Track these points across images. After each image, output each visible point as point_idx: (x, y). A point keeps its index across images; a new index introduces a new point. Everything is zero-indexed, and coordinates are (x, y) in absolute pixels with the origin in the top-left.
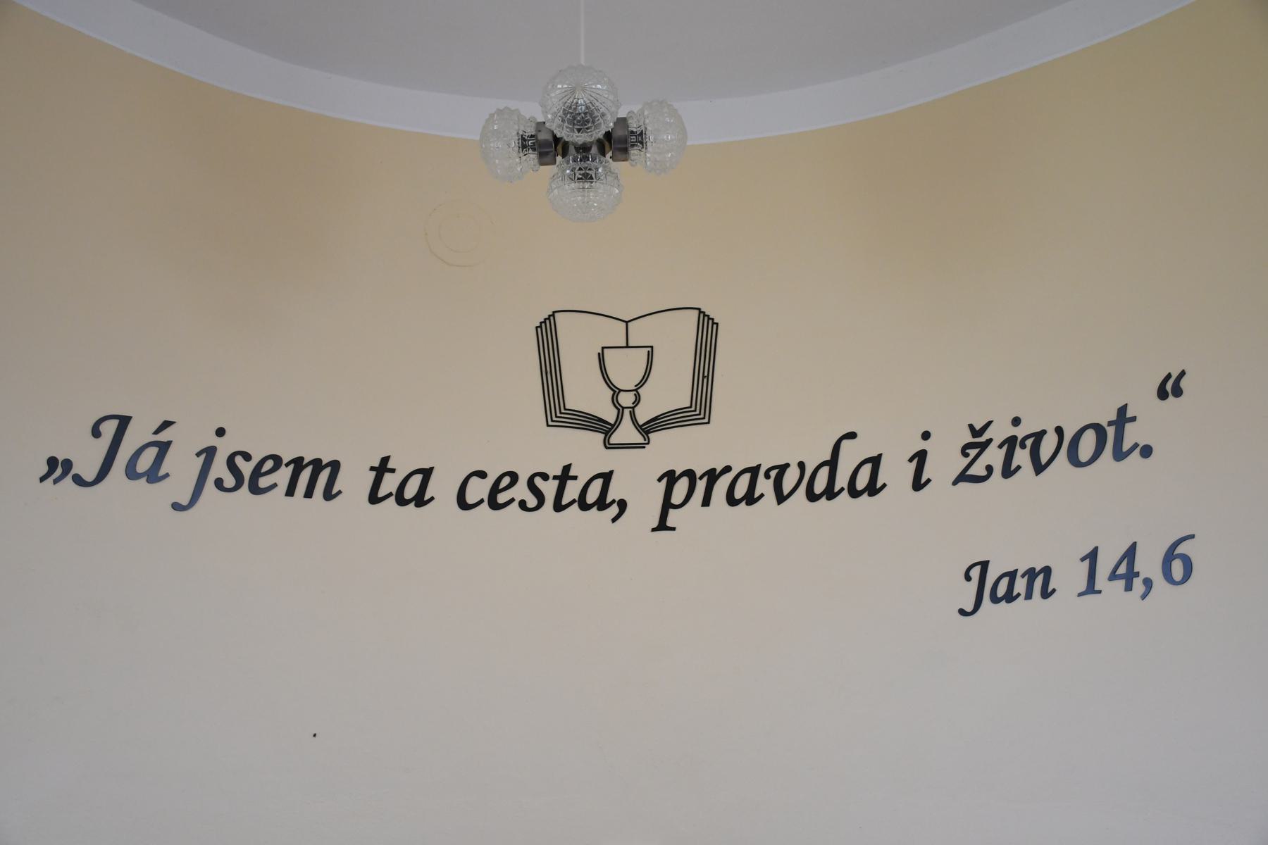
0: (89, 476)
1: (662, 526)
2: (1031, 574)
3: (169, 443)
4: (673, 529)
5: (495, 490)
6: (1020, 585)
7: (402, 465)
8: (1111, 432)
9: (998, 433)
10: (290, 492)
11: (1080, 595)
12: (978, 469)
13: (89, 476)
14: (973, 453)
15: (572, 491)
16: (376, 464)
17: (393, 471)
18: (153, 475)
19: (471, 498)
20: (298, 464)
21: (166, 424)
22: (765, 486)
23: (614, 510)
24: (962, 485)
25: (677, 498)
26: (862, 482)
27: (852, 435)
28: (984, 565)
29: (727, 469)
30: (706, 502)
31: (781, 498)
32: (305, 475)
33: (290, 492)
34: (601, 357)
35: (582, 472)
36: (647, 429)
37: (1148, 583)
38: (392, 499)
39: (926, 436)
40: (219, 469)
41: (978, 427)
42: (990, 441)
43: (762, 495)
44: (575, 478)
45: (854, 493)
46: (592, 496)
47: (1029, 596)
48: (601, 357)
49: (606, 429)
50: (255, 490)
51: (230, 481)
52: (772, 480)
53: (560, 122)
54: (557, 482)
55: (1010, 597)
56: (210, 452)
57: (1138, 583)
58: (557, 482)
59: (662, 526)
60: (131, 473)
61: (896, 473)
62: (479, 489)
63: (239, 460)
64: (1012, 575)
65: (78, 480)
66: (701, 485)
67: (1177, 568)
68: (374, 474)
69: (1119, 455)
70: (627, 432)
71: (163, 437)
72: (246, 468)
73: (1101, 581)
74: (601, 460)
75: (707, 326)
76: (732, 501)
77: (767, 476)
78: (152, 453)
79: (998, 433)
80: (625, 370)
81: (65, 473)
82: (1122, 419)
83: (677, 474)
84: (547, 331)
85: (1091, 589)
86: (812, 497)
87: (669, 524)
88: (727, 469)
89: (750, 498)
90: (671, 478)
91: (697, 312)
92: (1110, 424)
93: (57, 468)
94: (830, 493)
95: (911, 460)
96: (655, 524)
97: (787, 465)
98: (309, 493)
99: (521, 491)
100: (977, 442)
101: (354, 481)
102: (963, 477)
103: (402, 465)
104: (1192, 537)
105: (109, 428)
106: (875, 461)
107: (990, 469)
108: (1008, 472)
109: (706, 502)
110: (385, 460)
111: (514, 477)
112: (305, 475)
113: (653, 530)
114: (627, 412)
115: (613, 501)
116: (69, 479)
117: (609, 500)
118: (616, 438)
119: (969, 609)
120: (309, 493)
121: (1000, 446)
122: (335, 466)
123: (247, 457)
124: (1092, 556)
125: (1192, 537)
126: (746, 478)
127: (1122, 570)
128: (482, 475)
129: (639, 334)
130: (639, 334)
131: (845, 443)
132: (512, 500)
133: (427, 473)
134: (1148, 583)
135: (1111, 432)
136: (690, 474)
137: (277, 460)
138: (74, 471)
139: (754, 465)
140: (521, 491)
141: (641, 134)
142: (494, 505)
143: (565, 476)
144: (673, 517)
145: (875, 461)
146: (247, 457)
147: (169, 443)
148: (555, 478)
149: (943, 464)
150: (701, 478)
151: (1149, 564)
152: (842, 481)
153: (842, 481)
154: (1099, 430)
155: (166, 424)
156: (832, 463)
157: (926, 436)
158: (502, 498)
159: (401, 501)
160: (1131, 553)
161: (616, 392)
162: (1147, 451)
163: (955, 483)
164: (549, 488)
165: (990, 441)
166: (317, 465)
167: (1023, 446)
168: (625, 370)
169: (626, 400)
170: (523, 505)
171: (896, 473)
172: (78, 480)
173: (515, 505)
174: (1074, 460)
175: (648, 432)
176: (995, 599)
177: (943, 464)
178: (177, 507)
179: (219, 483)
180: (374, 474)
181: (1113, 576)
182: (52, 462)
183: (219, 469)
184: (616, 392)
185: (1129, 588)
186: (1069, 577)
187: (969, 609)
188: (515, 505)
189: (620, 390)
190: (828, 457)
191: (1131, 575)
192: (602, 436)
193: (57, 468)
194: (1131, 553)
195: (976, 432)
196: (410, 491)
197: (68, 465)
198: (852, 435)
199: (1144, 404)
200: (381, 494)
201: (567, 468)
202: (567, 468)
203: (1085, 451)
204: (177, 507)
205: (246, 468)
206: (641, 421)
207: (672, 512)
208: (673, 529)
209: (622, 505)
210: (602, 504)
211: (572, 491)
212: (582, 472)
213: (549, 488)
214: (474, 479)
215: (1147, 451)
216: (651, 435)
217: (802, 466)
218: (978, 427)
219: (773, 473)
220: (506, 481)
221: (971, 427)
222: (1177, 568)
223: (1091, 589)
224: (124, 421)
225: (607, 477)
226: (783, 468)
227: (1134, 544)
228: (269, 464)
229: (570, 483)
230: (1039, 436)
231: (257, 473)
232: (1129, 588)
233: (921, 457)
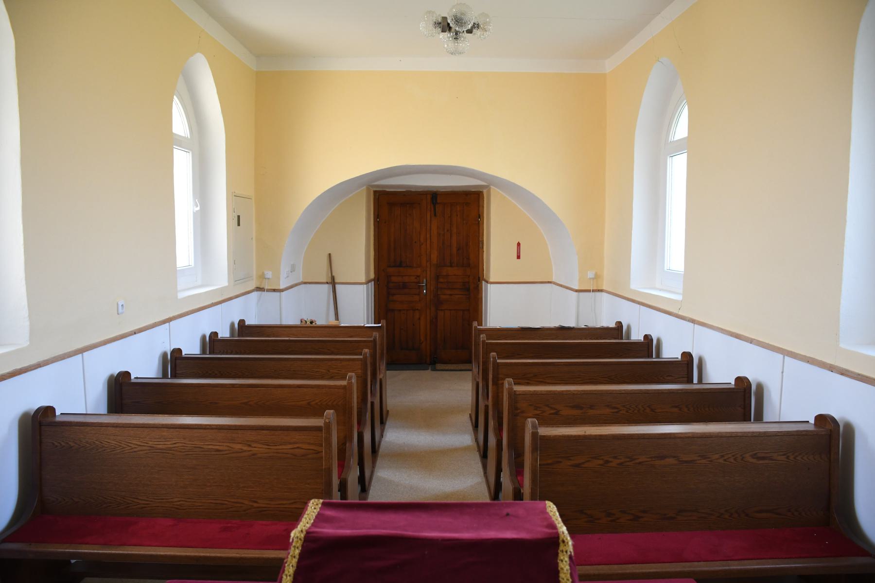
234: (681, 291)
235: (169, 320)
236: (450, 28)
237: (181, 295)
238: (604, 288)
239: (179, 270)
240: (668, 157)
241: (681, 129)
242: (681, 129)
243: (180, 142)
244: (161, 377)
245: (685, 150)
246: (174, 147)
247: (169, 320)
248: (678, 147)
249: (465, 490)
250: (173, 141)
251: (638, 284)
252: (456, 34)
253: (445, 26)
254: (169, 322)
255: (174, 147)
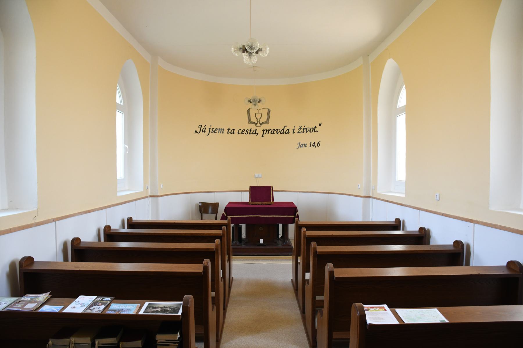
0: (199, 133)
1: (263, 136)
2: (304, 144)
5: (242, 132)
6: (303, 145)
8: (314, 129)
10: (219, 133)
12: (300, 132)
13: (199, 133)
14: (300, 129)
15: (252, 132)
18: (205, 132)
19: (239, 133)
21: (205, 126)
22: (275, 132)
23: (257, 134)
25: (264, 133)
26: (287, 132)
27: (286, 126)
28: (300, 143)
29: (271, 129)
30: (268, 134)
32: (220, 130)
33: (219, 133)
35: (253, 130)
36: (261, 124)
37: (316, 146)
39: (295, 127)
40: (211, 130)
45: (286, 133)
46: (254, 132)
47: (304, 147)
49: (256, 124)
50: (215, 133)
51: (212, 132)
53: (246, 54)
55: (302, 147)
56: (210, 128)
57: (315, 146)
59: (263, 136)
60: (203, 132)
62: (240, 132)
63: (213, 129)
64: (303, 144)
65: (198, 133)
66: (268, 131)
67: (318, 145)
69: (315, 132)
70: (258, 124)
72: (214, 130)
76: (271, 133)
77: (276, 131)
78: (204, 129)
79: (303, 127)
80: (258, 116)
82: (315, 127)
85: (310, 147)
86: (281, 133)
87: (264, 136)
88: (271, 129)
89: (274, 133)
90: (264, 130)
93: (196, 132)
94: (283, 133)
98: (221, 133)
99: (245, 132)
100: (300, 129)
102: (298, 132)
103: (231, 129)
105: (200, 127)
106: (289, 130)
107: (301, 132)
108: (303, 132)
109: (268, 134)
111: (244, 130)
120: (221, 133)
123: (214, 129)
124: (311, 143)
126: (273, 131)
127: (313, 145)
128: (241, 130)
129: (260, 112)
130: (260, 112)
133: (234, 130)
134: (316, 146)
135: (314, 129)
137: (217, 129)
140: (245, 132)
141: (261, 49)
142: (242, 134)
143: (251, 130)
145: (289, 130)
146: (214, 129)
149: (296, 131)
151: (316, 144)
152: (284, 132)
153: (284, 132)
155: (205, 126)
156: (284, 129)
158: (243, 133)
160: (314, 143)
161: (257, 119)
162: (317, 132)
164: (249, 131)
166: (221, 129)
168: (258, 116)
169: (258, 120)
170: (246, 133)
171: (291, 131)
172: (198, 133)
177: (296, 131)
178: (207, 135)
179: (211, 132)
181: (313, 145)
183: (211, 130)
184: (257, 119)
186: (308, 145)
187: (298, 148)
190: (283, 129)
191: (314, 145)
194: (314, 143)
195: (300, 127)
196: (232, 132)
197: (197, 131)
198: (286, 126)
199: (317, 126)
201: (251, 129)
202: (251, 129)
203: (311, 131)
204: (207, 135)
205: (214, 130)
209: (258, 134)
210: (255, 133)
211: (252, 132)
212: (253, 130)
213: (249, 131)
214: (240, 130)
215: (317, 132)
222: (318, 145)
224: (201, 126)
225: (256, 130)
228: (216, 129)
230: (307, 128)
231: (215, 131)
233: (294, 129)
234: (404, 192)
235: (106, 207)
236: (247, 52)
237: (119, 194)
238: (371, 195)
239: (118, 179)
240: (397, 117)
241: (402, 101)
242: (402, 101)
243: (121, 108)
244: (7, 207)
245: (404, 112)
246: (117, 110)
247: (106, 207)
248: (402, 110)
249: (238, 336)
250: (116, 107)
251: (381, 190)
252: (250, 54)
253: (244, 50)
254: (106, 209)
255: (117, 110)
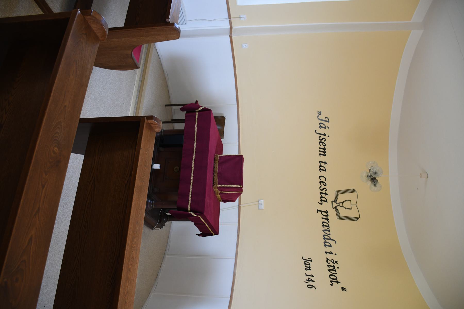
0: (319, 117)
1: (318, 211)
2: (309, 267)
3: (326, 128)
4: (317, 212)
5: (323, 182)
7: (326, 166)
8: (336, 281)
9: (336, 265)
10: (320, 148)
11: (306, 274)
12: (329, 261)
13: (319, 118)
14: (332, 261)
15: (324, 195)
16: (326, 162)
17: (325, 165)
18: (320, 127)
19: (321, 178)
20: (325, 149)
21: (329, 128)
23: (321, 203)
24: (326, 259)
25: (323, 213)
27: (336, 243)
28: (311, 261)
30: (322, 218)
31: (324, 231)
33: (320, 148)
34: (349, 200)
35: (327, 197)
36: (335, 208)
37: (308, 283)
38: (320, 165)
40: (322, 137)
41: (337, 262)
42: (334, 264)
43: (324, 227)
44: (326, 196)
46: (323, 199)
47: (305, 267)
48: (349, 200)
49: (335, 201)
50: (320, 143)
51: (321, 138)
52: (327, 229)
54: (325, 193)
55: (305, 264)
56: (325, 135)
58: (325, 193)
61: (329, 249)
62: (323, 179)
63: (324, 140)
64: (309, 265)
65: (318, 116)
66: (326, 217)
68: (324, 162)
70: (335, 205)
71: (327, 128)
72: (323, 141)
73: (308, 277)
74: (330, 200)
75: (357, 219)
76: (323, 222)
77: (328, 228)
78: (324, 126)
79: (336, 265)
80: (347, 204)
81: (319, 114)
82: (338, 282)
83: (328, 213)
84: (353, 191)
85: (306, 275)
87: (318, 212)
89: (323, 226)
91: (359, 217)
92: (337, 281)
93: (320, 113)
94: (324, 239)
95: (331, 252)
96: (318, 209)
97: (330, 232)
98: (320, 151)
99: (323, 187)
101: (323, 158)
102: (327, 259)
103: (326, 166)
104: (316, 289)
105: (327, 119)
106: (331, 246)
107: (329, 263)
109: (322, 218)
110: (327, 163)
111: (325, 185)
112: (323, 150)
113: (317, 209)
114: (339, 205)
115: (322, 202)
116: (318, 115)
117: (322, 202)
118: (333, 203)
119: (303, 258)
120: (320, 151)
121: (333, 265)
122: (325, 155)
123: (325, 141)
124: (312, 276)
125: (316, 289)
127: (310, 280)
128: (325, 180)
131: (334, 242)
132: (321, 185)
133: (325, 170)
135: (336, 281)
136: (328, 215)
137: (325, 146)
138: (320, 115)
139: (330, 226)
140: (323, 187)
142: (320, 182)
143: (326, 194)
144: (320, 213)
145: (331, 246)
146: (325, 141)
147: (326, 128)
148: (326, 192)
149: (330, 257)
150: (327, 217)
151: (310, 283)
152: (327, 241)
153: (327, 241)
154: (336, 279)
155: (329, 128)
156: (330, 239)
157: (336, 254)
158: (322, 183)
159: (320, 166)
160: (313, 281)
161: (342, 203)
163: (326, 258)
164: (324, 191)
165: (334, 264)
166: (325, 152)
167: (333, 268)
168: (347, 204)
169: (341, 205)
170: (321, 187)
171: (329, 249)
172: (318, 116)
173: (321, 186)
174: (330, 275)
175: (335, 208)
176: (305, 262)
177: (330, 257)
178: (316, 131)
179: (320, 137)
180: (324, 162)
181: (309, 278)
182: (320, 112)
183: (322, 137)
185: (307, 280)
187: (303, 258)
188: (321, 186)
189: (343, 204)
190: (331, 238)
192: (334, 200)
193: (320, 113)
194: (313, 281)
195: (336, 262)
196: (322, 168)
197: (320, 114)
198: (336, 243)
200: (321, 163)
204: (316, 131)
205: (323, 141)
206: (337, 207)
207: (320, 212)
208: (317, 212)
209: (321, 204)
210: (321, 200)
211: (324, 195)
212: (327, 197)
213: (324, 191)
216: (334, 209)
217: (330, 234)
218: (337, 262)
219: (328, 230)
220: (325, 184)
221: (337, 261)
223: (306, 275)
224: (328, 122)
225: (326, 201)
226: (329, 231)
227: (314, 277)
228: (324, 144)
229: (325, 195)
230: (335, 271)
231: (322, 143)
232: (307, 280)
233: (332, 253)
